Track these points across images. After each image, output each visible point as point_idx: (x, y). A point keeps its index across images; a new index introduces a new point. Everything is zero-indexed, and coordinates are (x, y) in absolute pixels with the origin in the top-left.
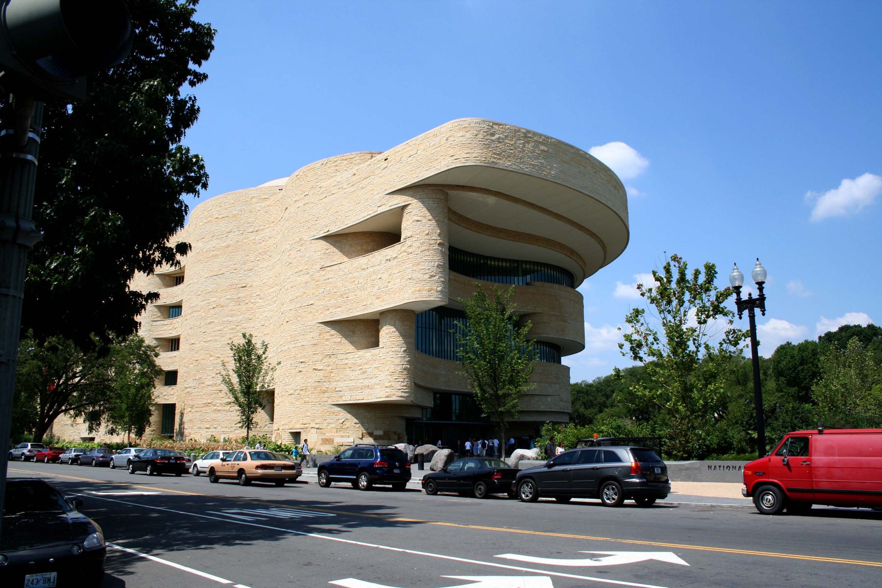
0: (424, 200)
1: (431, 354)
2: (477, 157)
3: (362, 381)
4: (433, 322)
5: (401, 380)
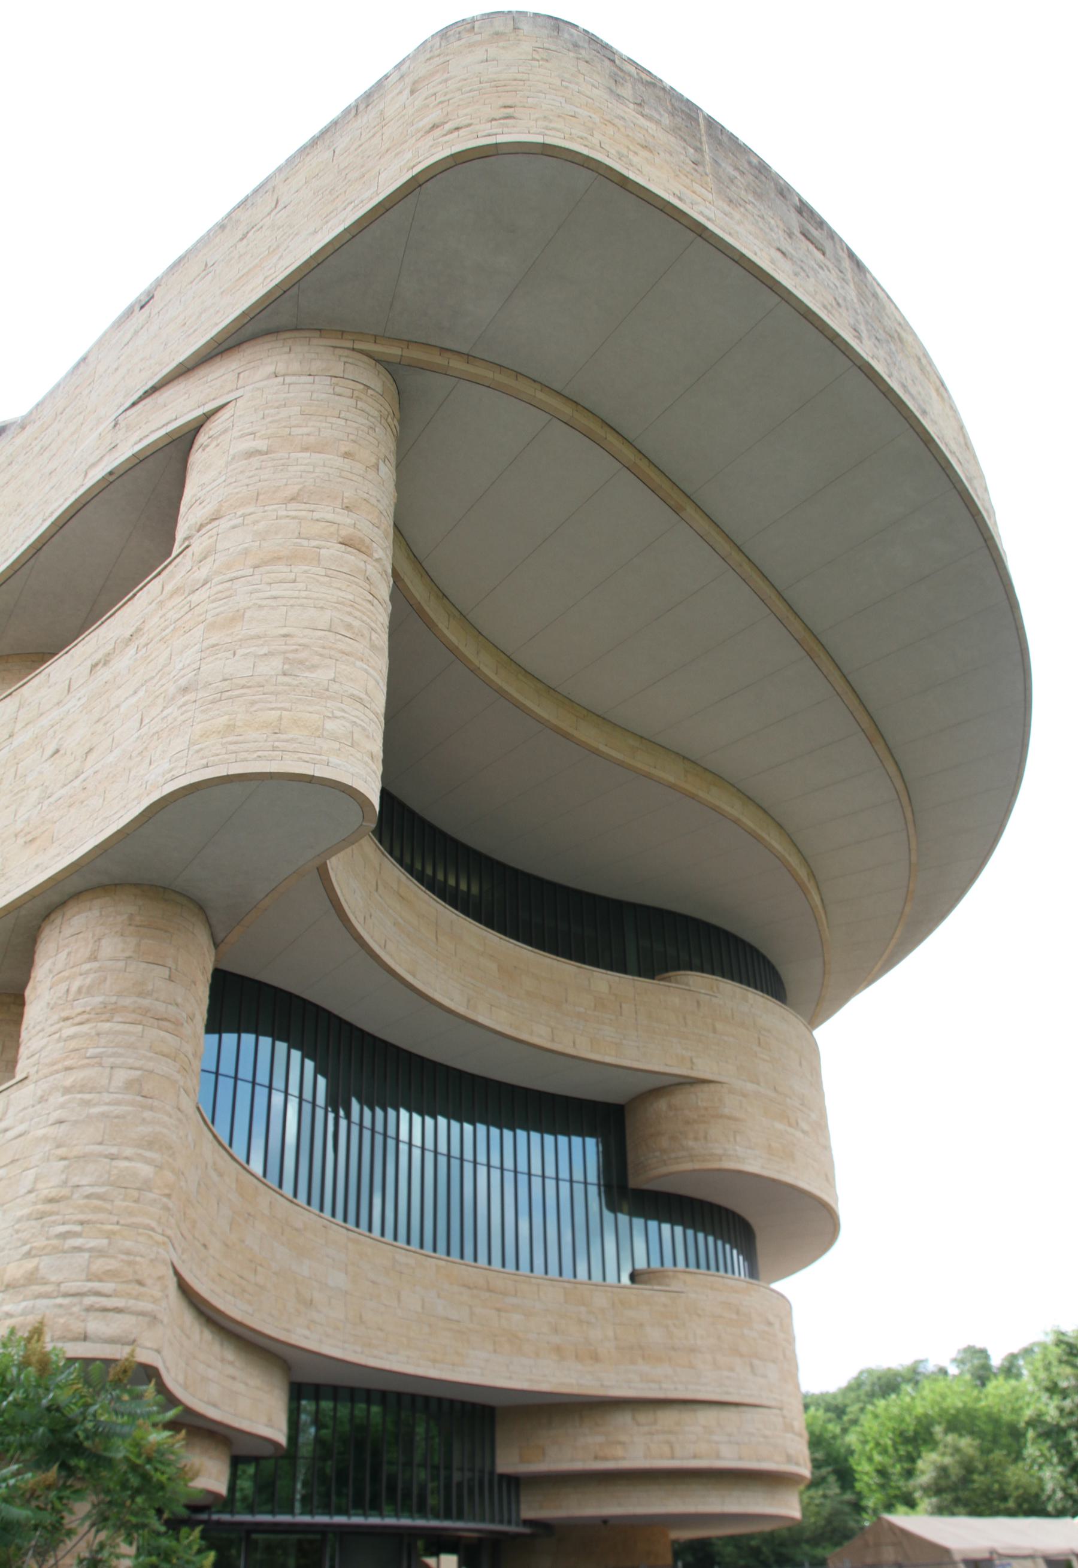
0: (288, 379)
1: (364, 1227)
5: (92, 1243)
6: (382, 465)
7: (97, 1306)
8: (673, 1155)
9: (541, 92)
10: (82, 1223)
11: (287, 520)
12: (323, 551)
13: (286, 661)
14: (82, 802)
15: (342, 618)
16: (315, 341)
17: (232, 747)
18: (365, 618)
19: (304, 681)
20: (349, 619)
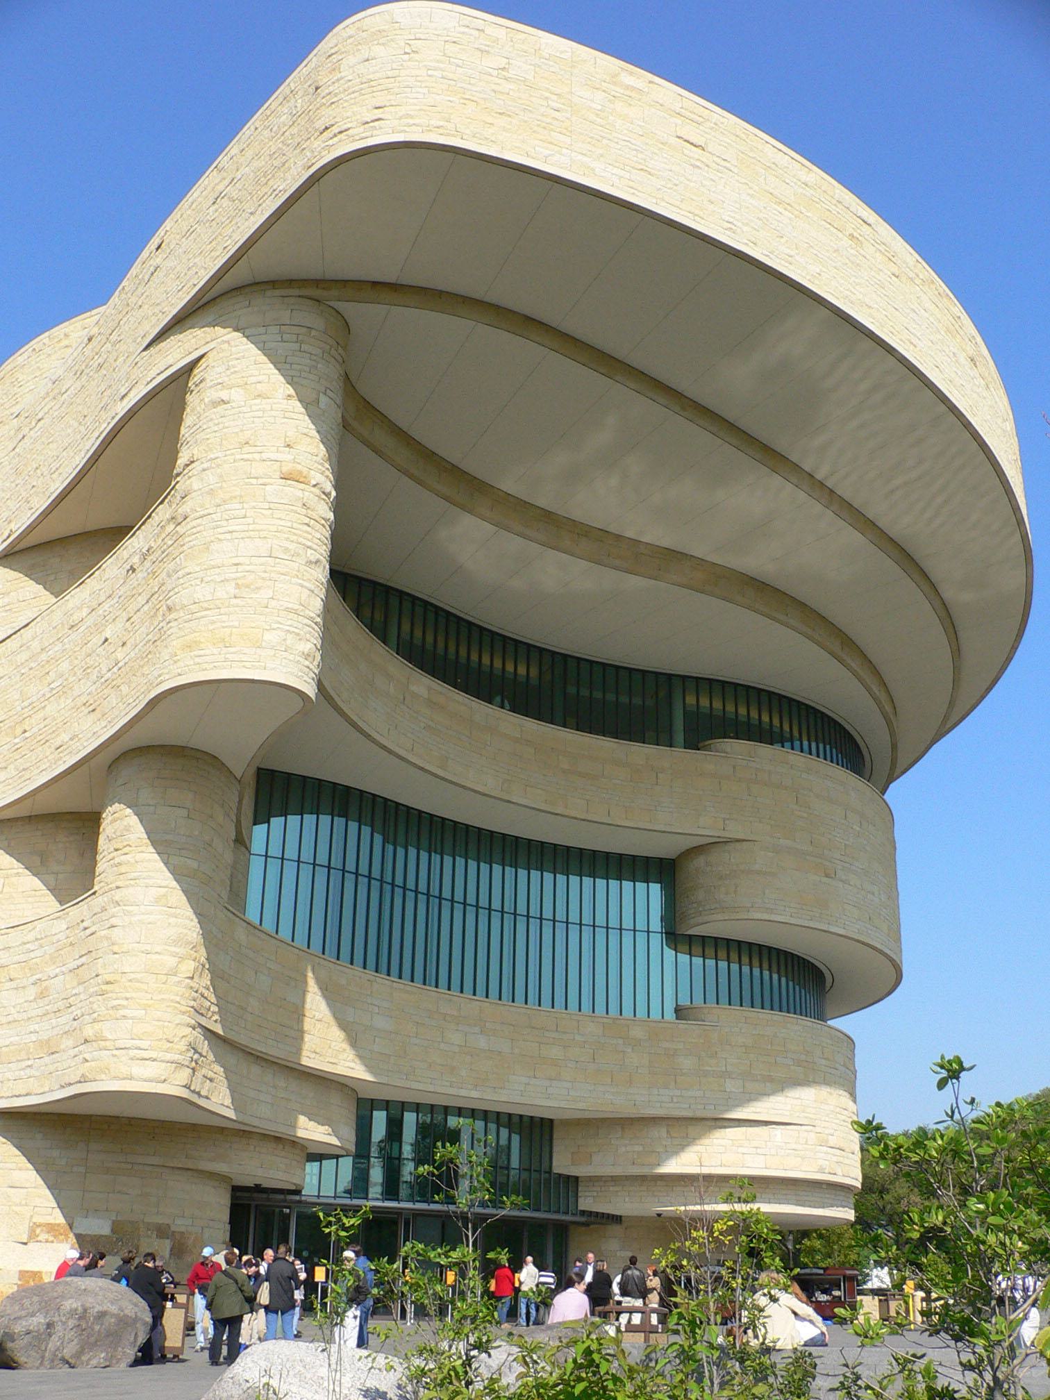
2: (412, 117)
3: (36, 1027)
4: (794, 997)
6: (323, 399)
7: (138, 1056)
8: (707, 907)
9: (408, 87)
10: (127, 999)
11: (242, 463)
12: (268, 488)
13: (238, 586)
14: (118, 687)
15: (281, 544)
16: (269, 293)
17: (197, 660)
18: (301, 540)
19: (250, 601)
20: (287, 544)
